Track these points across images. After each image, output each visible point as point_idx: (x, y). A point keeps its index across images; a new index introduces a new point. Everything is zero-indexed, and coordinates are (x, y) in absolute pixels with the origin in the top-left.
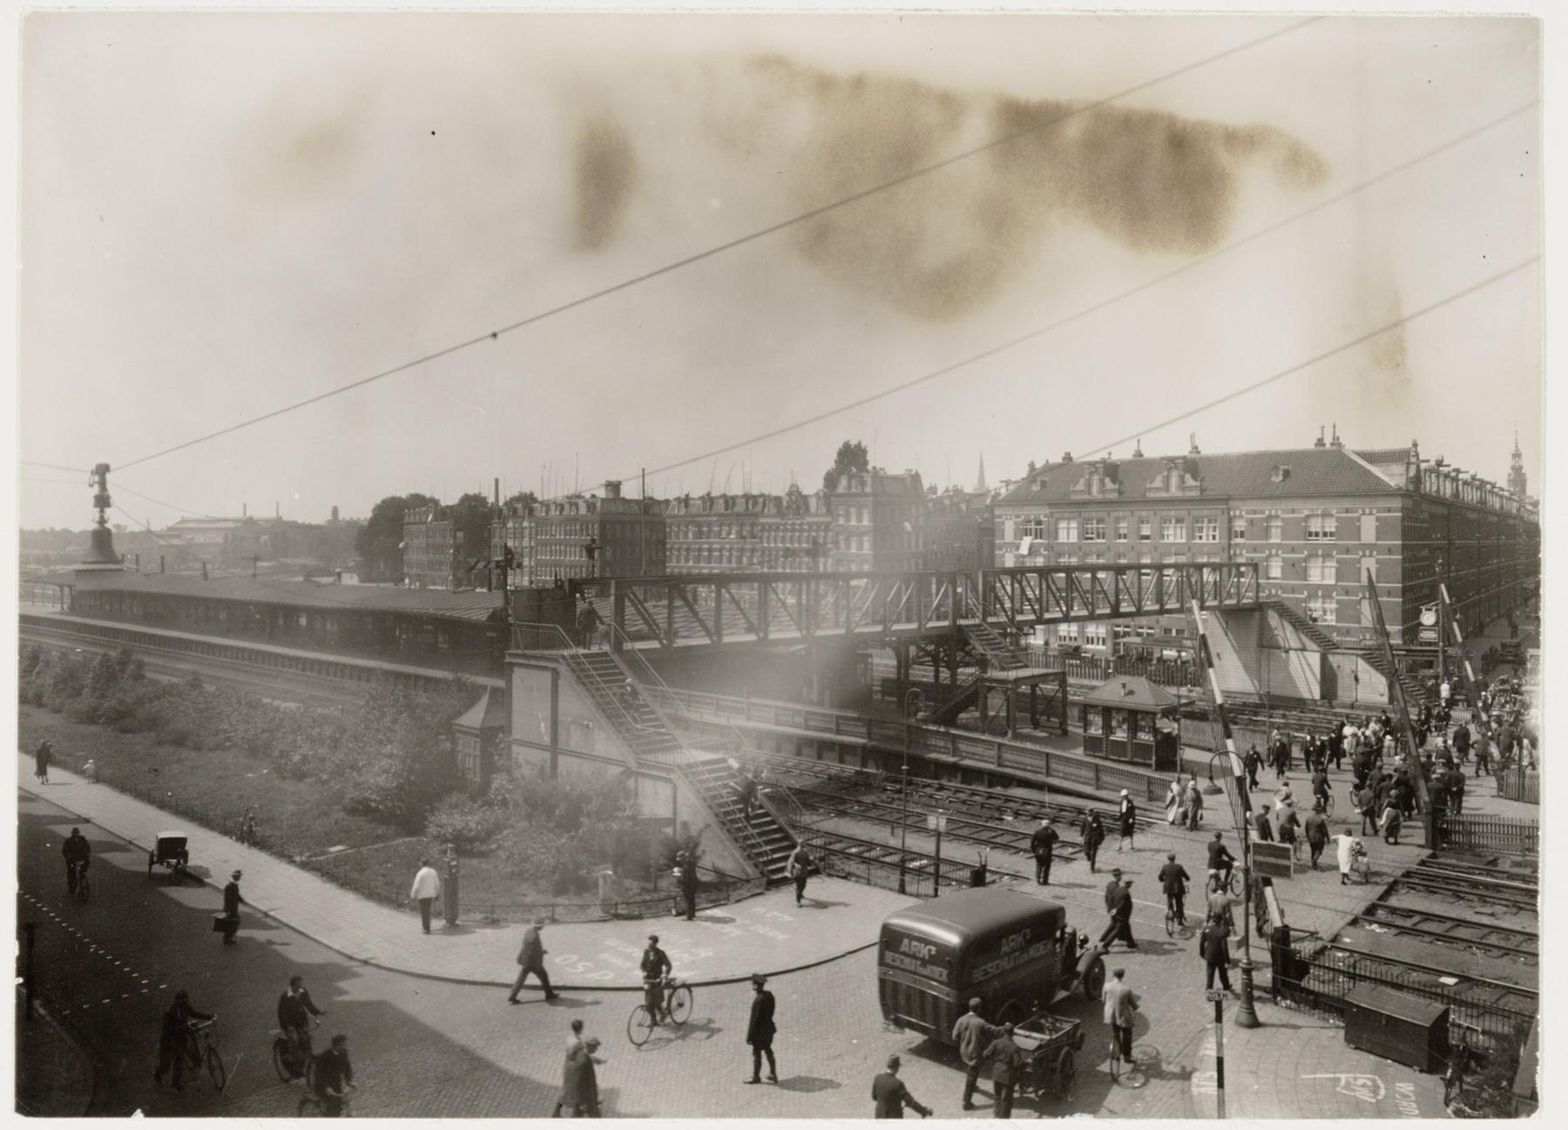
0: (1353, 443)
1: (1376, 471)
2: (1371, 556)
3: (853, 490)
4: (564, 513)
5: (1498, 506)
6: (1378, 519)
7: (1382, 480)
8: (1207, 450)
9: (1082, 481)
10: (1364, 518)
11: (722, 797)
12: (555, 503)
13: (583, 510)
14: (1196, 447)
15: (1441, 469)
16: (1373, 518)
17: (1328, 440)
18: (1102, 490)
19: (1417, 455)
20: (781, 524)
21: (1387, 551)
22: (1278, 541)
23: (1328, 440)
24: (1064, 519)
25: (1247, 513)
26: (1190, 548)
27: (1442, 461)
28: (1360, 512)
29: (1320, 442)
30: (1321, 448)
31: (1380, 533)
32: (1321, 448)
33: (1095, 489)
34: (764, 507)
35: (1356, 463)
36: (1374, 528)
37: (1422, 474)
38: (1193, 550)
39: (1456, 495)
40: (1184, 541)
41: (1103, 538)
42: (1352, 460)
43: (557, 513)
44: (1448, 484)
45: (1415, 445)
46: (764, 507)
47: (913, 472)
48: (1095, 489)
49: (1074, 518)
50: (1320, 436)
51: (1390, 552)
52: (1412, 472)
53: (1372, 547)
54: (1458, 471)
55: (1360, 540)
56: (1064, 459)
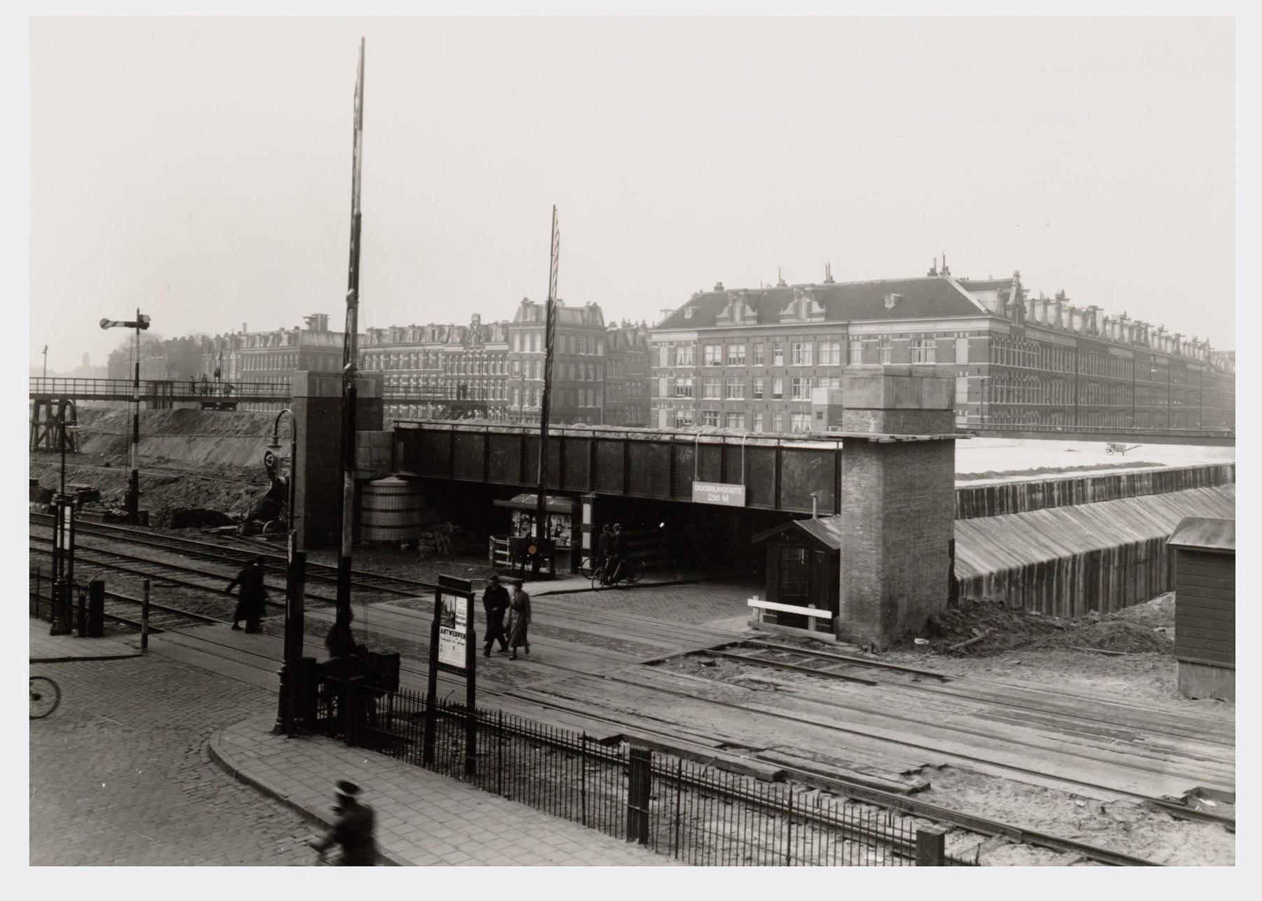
0: (957, 273)
1: (972, 297)
2: (964, 376)
3: (528, 320)
4: (269, 345)
5: (1156, 345)
6: (970, 342)
7: (975, 306)
8: (840, 279)
9: (726, 309)
10: (958, 341)
11: (451, 632)
12: (260, 335)
13: (285, 343)
14: (831, 278)
15: (1125, 322)
16: (966, 341)
17: (939, 270)
18: (744, 318)
19: (1209, 346)
20: (463, 353)
21: (976, 372)
22: (933, 363)
23: (939, 270)
24: (710, 345)
25: (863, 339)
26: (723, 372)
27: (1163, 328)
28: (956, 335)
29: (933, 272)
30: (934, 277)
31: (972, 355)
32: (934, 277)
33: (738, 317)
34: (449, 336)
35: (957, 290)
36: (967, 350)
37: (1150, 338)
38: (523, 358)
39: (1178, 352)
40: (810, 365)
41: (762, 363)
42: (954, 288)
43: (262, 345)
44: (1169, 344)
45: (1208, 340)
46: (449, 336)
47: (591, 304)
48: (738, 317)
49: (743, 344)
50: (933, 267)
51: (979, 372)
52: (1206, 354)
53: (964, 368)
54: (1179, 335)
55: (955, 361)
56: (716, 288)
